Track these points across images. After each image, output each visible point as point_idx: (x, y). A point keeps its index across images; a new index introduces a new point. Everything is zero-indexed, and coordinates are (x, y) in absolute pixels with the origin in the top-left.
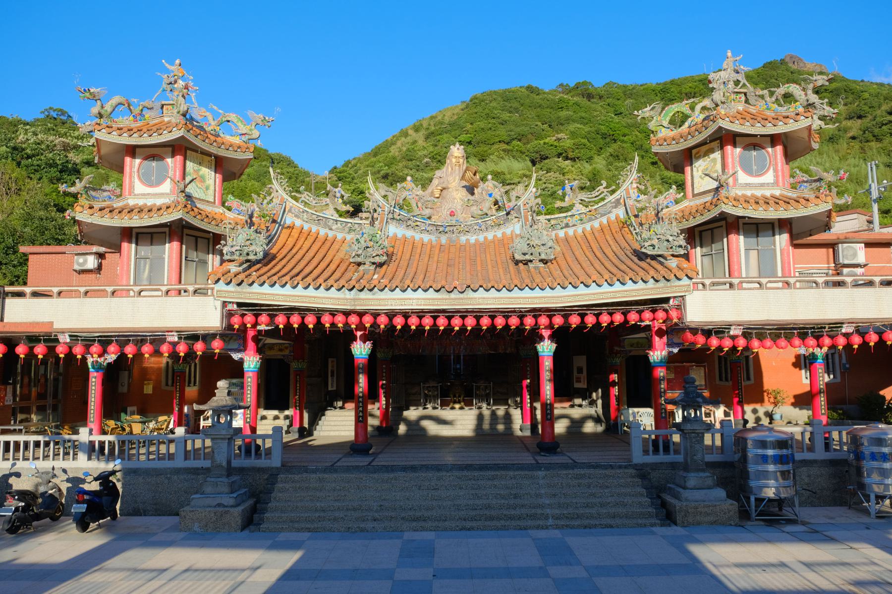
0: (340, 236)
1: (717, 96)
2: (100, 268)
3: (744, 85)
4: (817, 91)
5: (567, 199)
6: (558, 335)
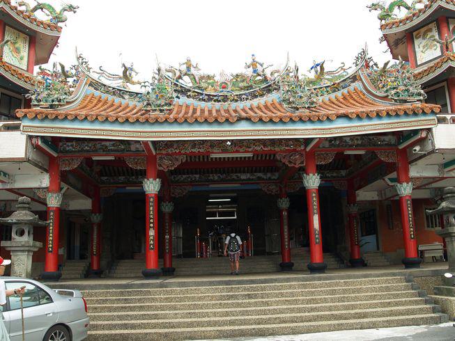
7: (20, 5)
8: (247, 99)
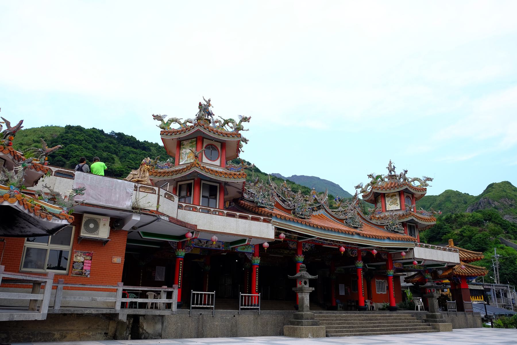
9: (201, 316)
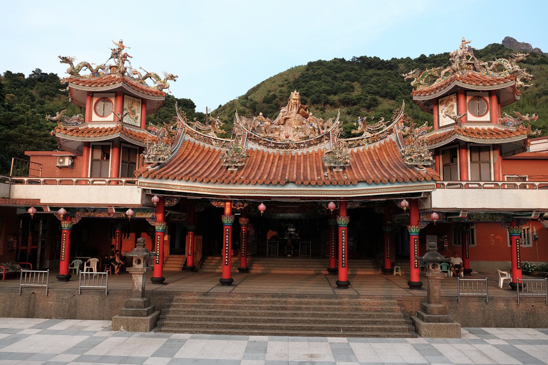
0: (217, 149)
1: (455, 66)
2: (73, 164)
3: (473, 58)
4: (518, 62)
5: (359, 128)
6: (350, 213)
7: (134, 74)
8: (304, 147)
9: (33, 295)
